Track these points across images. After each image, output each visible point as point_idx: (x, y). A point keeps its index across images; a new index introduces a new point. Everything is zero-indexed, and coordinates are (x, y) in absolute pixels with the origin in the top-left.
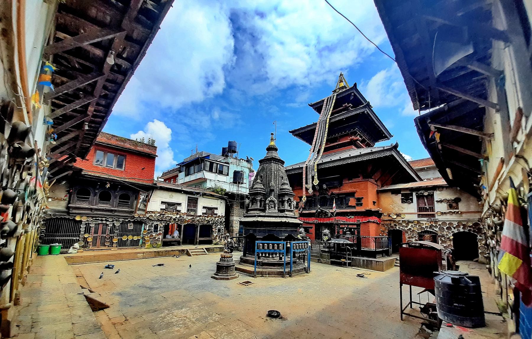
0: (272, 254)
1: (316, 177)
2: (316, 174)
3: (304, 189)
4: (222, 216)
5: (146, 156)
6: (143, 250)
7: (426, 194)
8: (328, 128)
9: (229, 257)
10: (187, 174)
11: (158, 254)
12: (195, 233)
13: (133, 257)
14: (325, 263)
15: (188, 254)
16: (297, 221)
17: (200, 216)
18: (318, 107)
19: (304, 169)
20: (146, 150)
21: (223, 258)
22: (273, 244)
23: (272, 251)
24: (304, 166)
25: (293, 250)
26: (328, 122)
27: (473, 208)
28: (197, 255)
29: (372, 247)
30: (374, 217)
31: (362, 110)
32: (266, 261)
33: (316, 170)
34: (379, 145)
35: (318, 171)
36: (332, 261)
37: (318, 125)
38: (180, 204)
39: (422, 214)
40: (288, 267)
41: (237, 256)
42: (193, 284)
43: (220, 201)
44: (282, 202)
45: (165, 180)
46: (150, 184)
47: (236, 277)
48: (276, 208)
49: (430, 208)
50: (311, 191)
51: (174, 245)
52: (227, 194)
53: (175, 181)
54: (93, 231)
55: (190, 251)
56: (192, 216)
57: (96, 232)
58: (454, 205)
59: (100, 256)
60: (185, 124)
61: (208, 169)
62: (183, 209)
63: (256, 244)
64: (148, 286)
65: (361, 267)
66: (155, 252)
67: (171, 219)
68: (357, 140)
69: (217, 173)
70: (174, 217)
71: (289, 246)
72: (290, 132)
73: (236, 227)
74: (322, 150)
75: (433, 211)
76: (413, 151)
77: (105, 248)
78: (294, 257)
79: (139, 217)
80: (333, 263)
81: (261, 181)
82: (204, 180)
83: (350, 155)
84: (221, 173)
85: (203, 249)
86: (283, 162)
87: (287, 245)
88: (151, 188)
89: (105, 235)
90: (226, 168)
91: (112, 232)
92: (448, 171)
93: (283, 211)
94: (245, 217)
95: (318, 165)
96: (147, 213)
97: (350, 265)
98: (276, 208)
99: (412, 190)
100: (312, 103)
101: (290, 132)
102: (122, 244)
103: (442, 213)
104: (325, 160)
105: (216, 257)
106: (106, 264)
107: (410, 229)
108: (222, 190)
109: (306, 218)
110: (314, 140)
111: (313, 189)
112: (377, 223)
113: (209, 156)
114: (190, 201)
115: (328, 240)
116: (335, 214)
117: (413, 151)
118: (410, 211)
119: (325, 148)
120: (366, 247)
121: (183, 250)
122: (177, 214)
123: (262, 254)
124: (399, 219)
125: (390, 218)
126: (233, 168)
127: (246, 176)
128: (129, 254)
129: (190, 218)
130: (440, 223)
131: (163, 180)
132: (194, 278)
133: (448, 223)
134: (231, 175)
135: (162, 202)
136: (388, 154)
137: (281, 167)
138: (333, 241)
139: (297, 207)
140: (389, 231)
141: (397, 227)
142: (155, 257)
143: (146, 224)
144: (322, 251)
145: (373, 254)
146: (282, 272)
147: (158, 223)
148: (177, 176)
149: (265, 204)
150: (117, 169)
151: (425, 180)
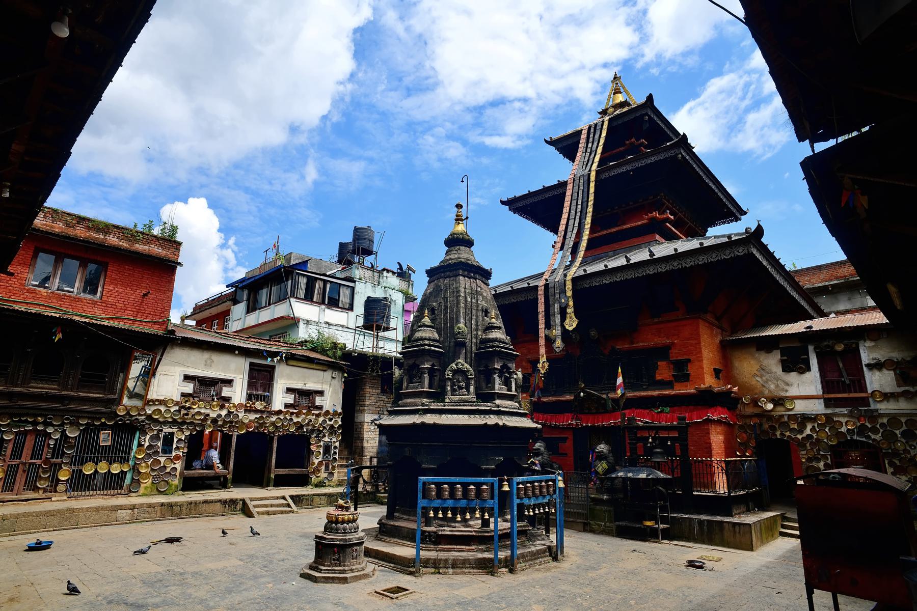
0: (463, 512)
2: (571, 303)
3: (542, 342)
4: (335, 413)
5: (154, 263)
6: (134, 500)
7: (840, 347)
8: (595, 192)
9: (349, 522)
10: (252, 308)
11: (171, 511)
12: (264, 457)
13: (108, 517)
15: (246, 512)
16: (527, 423)
17: (280, 412)
18: (567, 146)
19: (541, 291)
20: (156, 250)
21: (332, 524)
23: (463, 503)
24: (541, 283)
25: (516, 501)
26: (593, 178)
28: (268, 513)
31: (672, 153)
32: (447, 531)
33: (569, 294)
34: (718, 233)
36: (618, 527)
37: (570, 187)
38: (229, 382)
39: (835, 399)
40: (505, 547)
41: (369, 517)
42: (254, 593)
43: (328, 374)
44: (485, 376)
45: (199, 323)
46: (160, 333)
47: (366, 576)
48: (472, 389)
50: (559, 344)
51: (211, 487)
52: (348, 355)
53: (222, 325)
54: (9, 452)
55: (251, 504)
56: (257, 411)
57: (17, 454)
59: (17, 516)
60: (247, 190)
61: (302, 293)
62: (238, 393)
63: (420, 485)
64: (131, 600)
65: (695, 541)
66: (162, 505)
67: (205, 420)
69: (323, 303)
70: (213, 415)
71: (506, 488)
72: (503, 203)
73: (371, 440)
74: (584, 244)
75: (863, 388)
76: (803, 242)
77: (35, 495)
78: (521, 517)
79: (128, 413)
81: (432, 320)
82: (293, 322)
83: (676, 250)
84: (333, 303)
85: (284, 498)
86: (485, 274)
87: (501, 486)
88: (160, 343)
89: (38, 462)
91: (57, 452)
93: (491, 397)
94: (391, 413)
95: (574, 280)
96: (148, 403)
97: (668, 535)
98: (472, 389)
99: (810, 336)
100: (555, 137)
101: (503, 203)
102: (80, 484)
103: (886, 397)
104: (591, 269)
105: (314, 521)
106: (32, 539)
108: (335, 346)
109: (549, 416)
110: (563, 222)
111: (563, 340)
112: (727, 424)
113: (306, 262)
116: (622, 404)
117: (803, 242)
118: (805, 389)
119: (589, 240)
121: (233, 502)
122: (222, 407)
123: (436, 511)
124: (780, 411)
125: (757, 411)
126: (364, 291)
127: (396, 310)
128: (97, 509)
129: (253, 416)
130: (885, 420)
131: (193, 323)
132: (256, 577)
133: (903, 420)
135: (187, 378)
136: (741, 251)
137: (482, 285)
138: (621, 474)
139: (525, 387)
141: (778, 433)
142: (162, 517)
143: (144, 433)
144: (593, 499)
145: (723, 505)
146: (490, 560)
147: (175, 429)
148: (227, 313)
149: (443, 380)
150: (83, 295)
151: (833, 315)
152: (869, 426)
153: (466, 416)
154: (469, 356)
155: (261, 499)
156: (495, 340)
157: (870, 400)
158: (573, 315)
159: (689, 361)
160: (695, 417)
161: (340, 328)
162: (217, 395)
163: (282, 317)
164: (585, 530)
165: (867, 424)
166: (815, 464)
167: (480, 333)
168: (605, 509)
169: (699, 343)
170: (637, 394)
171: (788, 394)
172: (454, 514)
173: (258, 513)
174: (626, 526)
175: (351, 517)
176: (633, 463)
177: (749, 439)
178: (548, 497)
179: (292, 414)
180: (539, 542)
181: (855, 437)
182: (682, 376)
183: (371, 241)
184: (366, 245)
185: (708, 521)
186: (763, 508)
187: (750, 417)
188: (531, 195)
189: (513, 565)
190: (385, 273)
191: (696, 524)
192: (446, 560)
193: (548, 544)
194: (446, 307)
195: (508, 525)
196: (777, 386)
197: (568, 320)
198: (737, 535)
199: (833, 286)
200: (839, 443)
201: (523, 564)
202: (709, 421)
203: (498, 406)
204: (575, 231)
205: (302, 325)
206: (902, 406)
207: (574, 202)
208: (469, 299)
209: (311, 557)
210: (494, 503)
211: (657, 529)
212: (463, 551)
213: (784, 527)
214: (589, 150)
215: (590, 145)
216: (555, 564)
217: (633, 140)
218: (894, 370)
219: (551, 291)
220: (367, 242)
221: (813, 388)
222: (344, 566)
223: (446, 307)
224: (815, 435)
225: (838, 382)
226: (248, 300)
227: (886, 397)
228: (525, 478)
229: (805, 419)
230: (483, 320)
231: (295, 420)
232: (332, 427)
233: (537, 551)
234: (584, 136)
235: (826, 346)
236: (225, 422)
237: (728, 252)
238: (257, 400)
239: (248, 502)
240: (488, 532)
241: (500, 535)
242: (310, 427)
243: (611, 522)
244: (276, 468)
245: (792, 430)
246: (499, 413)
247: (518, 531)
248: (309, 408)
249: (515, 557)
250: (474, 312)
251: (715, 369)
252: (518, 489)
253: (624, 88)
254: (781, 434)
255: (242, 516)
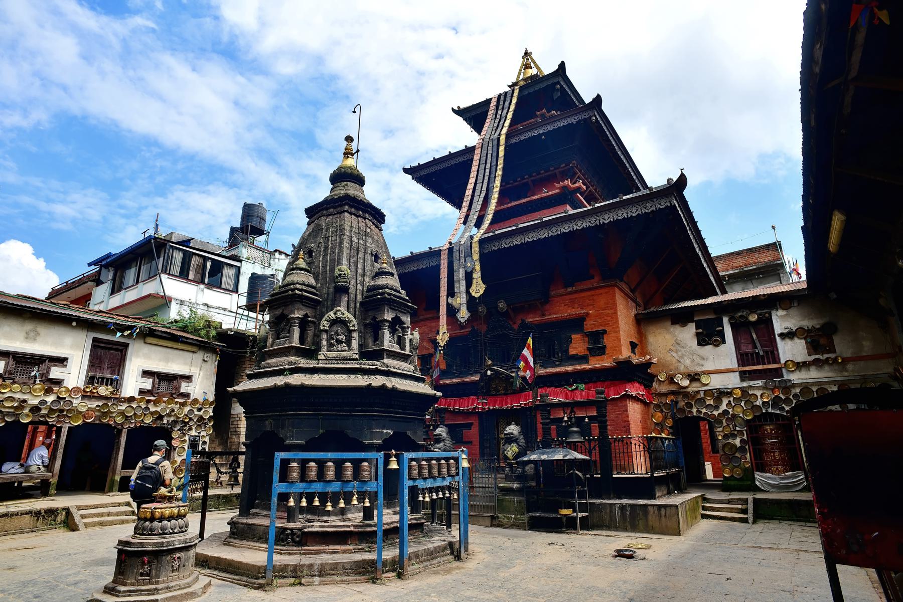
1: (477, 275)
2: (478, 268)
7: (753, 318)
8: (505, 156)
14: (514, 526)
15: (70, 524)
17: (131, 399)
18: (474, 116)
22: (339, 464)
23: (336, 487)
25: (408, 483)
27: (867, 347)
28: (102, 524)
29: (640, 467)
30: (637, 384)
32: (316, 527)
33: (476, 256)
35: (484, 259)
37: (478, 151)
38: (61, 361)
39: (750, 372)
40: (393, 545)
43: (200, 356)
44: (373, 328)
48: (355, 344)
49: (766, 352)
50: (463, 314)
52: (223, 335)
55: (77, 514)
56: (100, 397)
58: (822, 341)
61: (176, 270)
62: (74, 375)
65: (616, 528)
68: (578, 189)
70: (33, 401)
71: (394, 465)
74: (489, 217)
75: (776, 360)
80: (537, 525)
81: (309, 264)
87: (387, 462)
90: (232, 272)
92: (837, 221)
93: (378, 355)
97: (587, 525)
98: (355, 344)
101: (406, 171)
103: (799, 366)
107: (725, 412)
108: (209, 324)
114: (100, 352)
115: (517, 456)
119: (496, 213)
120: (623, 469)
121: (52, 512)
122: (48, 391)
124: (696, 387)
125: (673, 388)
129: (93, 404)
130: (797, 391)
133: (814, 389)
134: (244, 286)
136: (663, 204)
140: (675, 421)
141: (694, 410)
145: (644, 487)
146: (372, 563)
152: (783, 398)
153: (345, 376)
154: (352, 305)
155: (95, 507)
156: (386, 286)
157: (784, 370)
158: (480, 280)
159: (605, 332)
160: (611, 392)
161: (222, 312)
162: (41, 376)
163: (150, 295)
164: (492, 525)
165: (781, 396)
166: (731, 441)
167: (367, 280)
168: (515, 498)
169: (616, 313)
170: (550, 370)
171: (703, 369)
172: (323, 503)
173: (87, 525)
174: (539, 517)
175: (176, 511)
176: (547, 444)
177: (665, 418)
178: (449, 479)
179: (148, 401)
180: (437, 538)
181: (770, 410)
182: (597, 349)
183: (263, 219)
184: (255, 223)
185: (630, 505)
186: (682, 491)
187: (665, 395)
188: (435, 161)
189: (402, 568)
190: (277, 254)
191: (617, 509)
192: (311, 566)
193: (450, 539)
194: (326, 248)
195: (397, 517)
196: (693, 361)
197: (474, 287)
198: (663, 519)
199: (729, 276)
200: (755, 417)
201: (417, 566)
202: (628, 397)
203: (388, 366)
204: (483, 195)
205: (173, 303)
206: (813, 375)
207: (482, 167)
208: (355, 239)
209: (108, 574)
210: (376, 486)
211: (575, 518)
212: (336, 552)
213: (704, 508)
214: (498, 117)
215: (500, 112)
216: (457, 564)
217: (544, 110)
218: (805, 338)
219: (456, 255)
220: (258, 220)
221: (729, 361)
222: (157, 583)
223: (326, 248)
224: (730, 410)
225: (752, 354)
226: (114, 280)
227: (799, 366)
228: (419, 455)
229: (721, 394)
230: (373, 265)
231: (152, 409)
232: (201, 418)
233: (435, 548)
234: (493, 104)
235: (741, 316)
236: (51, 411)
237: (649, 205)
238: (102, 384)
239: (74, 511)
240: (371, 526)
241: (384, 531)
242: (172, 419)
243: (524, 514)
244: (123, 468)
245: (707, 407)
246: (388, 374)
247: (409, 525)
248: (172, 395)
249: (406, 557)
250: (361, 255)
251: (631, 342)
252: (410, 467)
253: (535, 63)
254: (698, 411)
255: (62, 530)
